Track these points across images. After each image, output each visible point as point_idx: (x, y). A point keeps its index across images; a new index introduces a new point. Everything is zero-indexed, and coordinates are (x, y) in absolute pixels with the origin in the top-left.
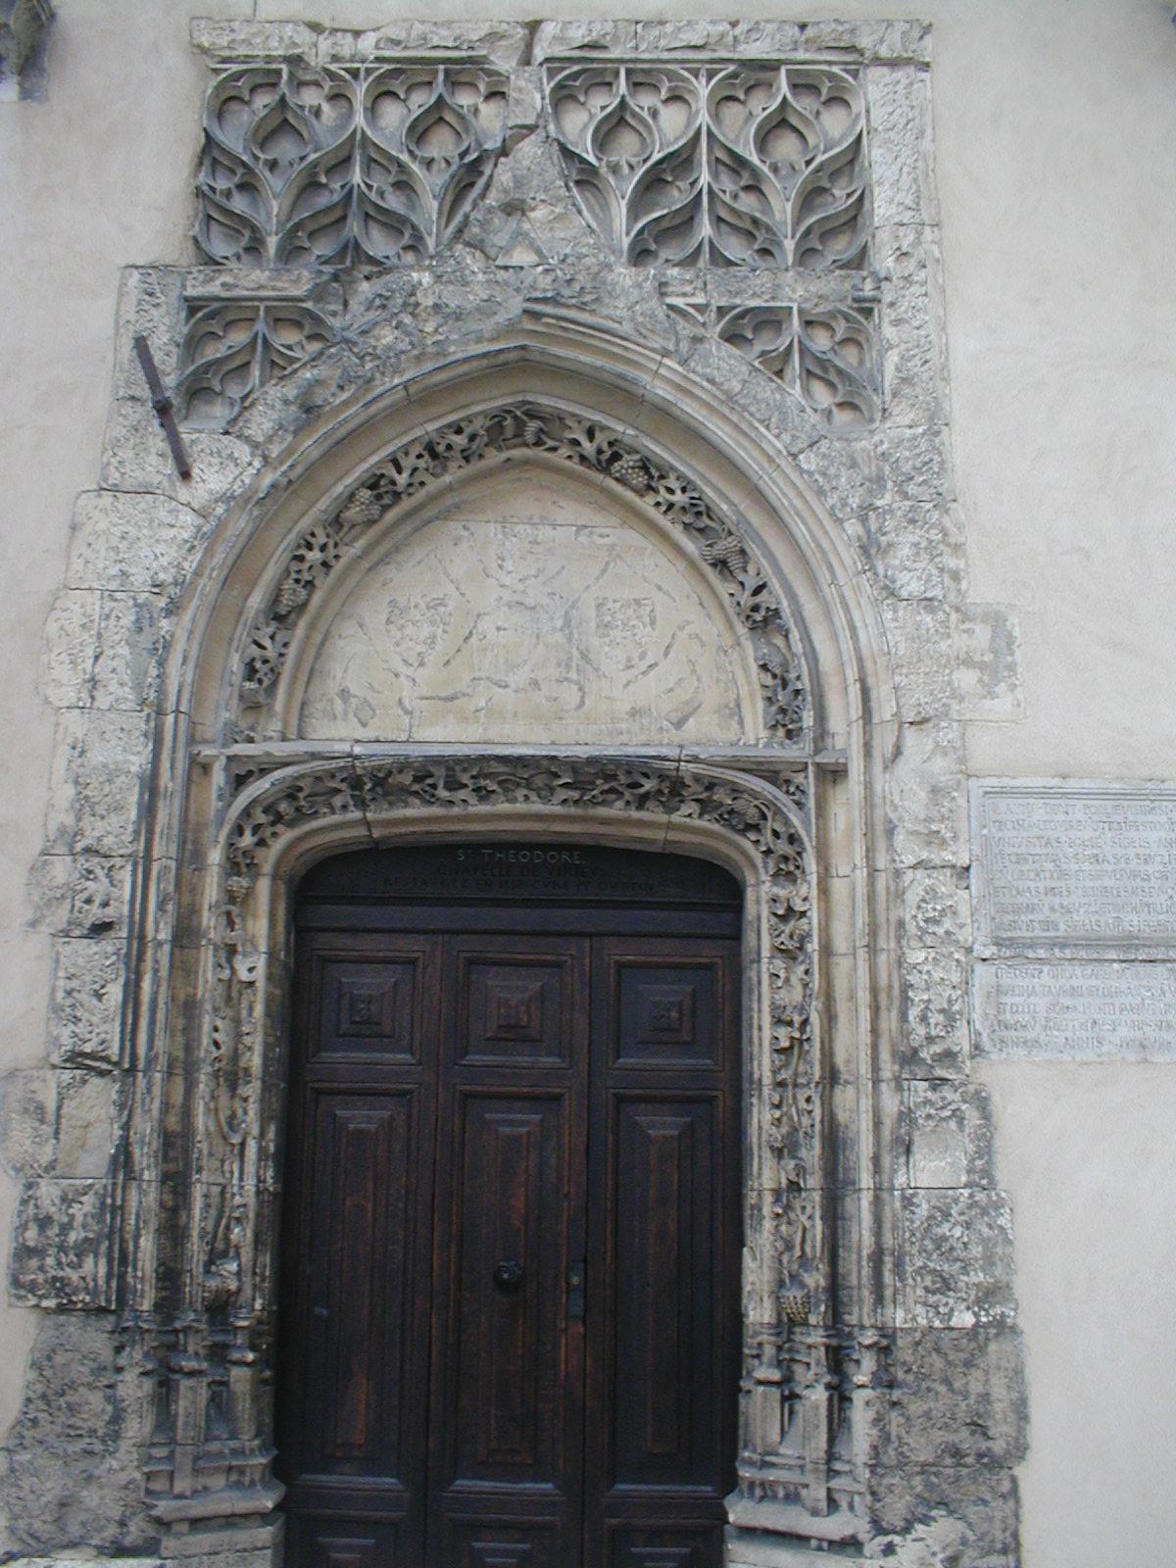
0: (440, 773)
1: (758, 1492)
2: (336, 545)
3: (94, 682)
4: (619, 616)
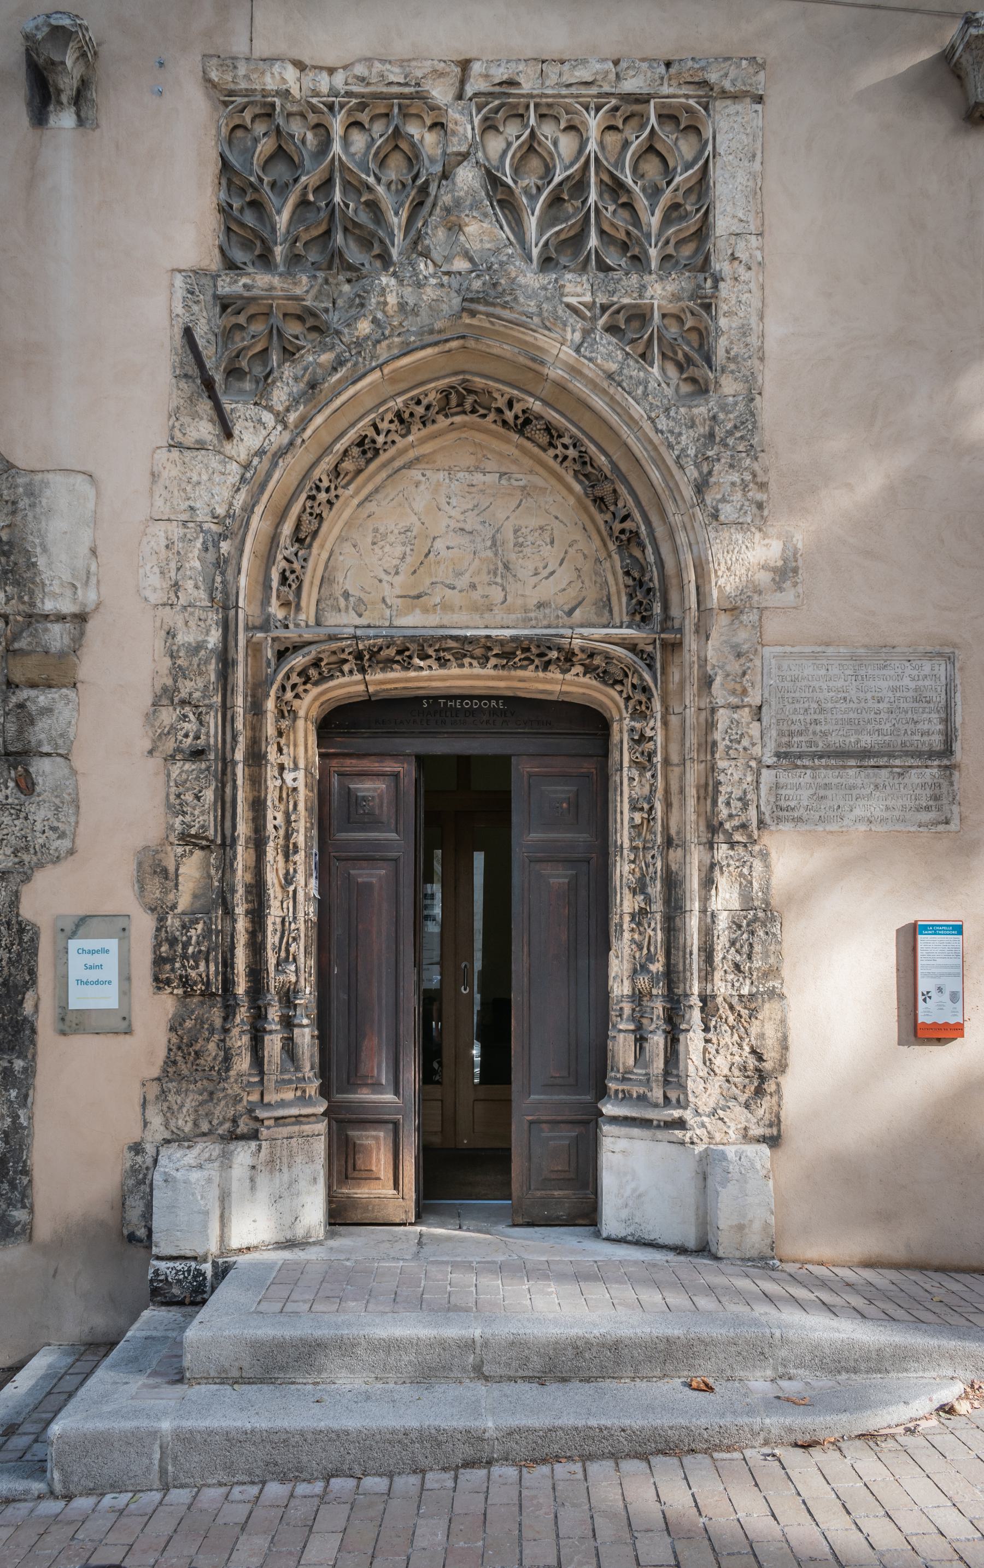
0: (413, 647)
1: (620, 1095)
2: (336, 488)
3: (176, 586)
4: (530, 538)
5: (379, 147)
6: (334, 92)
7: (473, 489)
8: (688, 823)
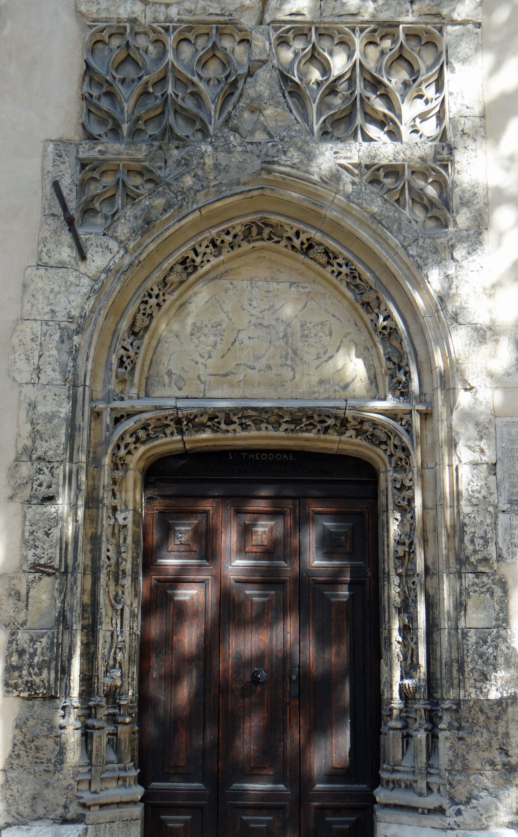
2: (164, 295)
3: (38, 370)
4: (313, 331)
5: (202, 56)
6: (169, 19)
7: (269, 295)
8: (440, 556)
